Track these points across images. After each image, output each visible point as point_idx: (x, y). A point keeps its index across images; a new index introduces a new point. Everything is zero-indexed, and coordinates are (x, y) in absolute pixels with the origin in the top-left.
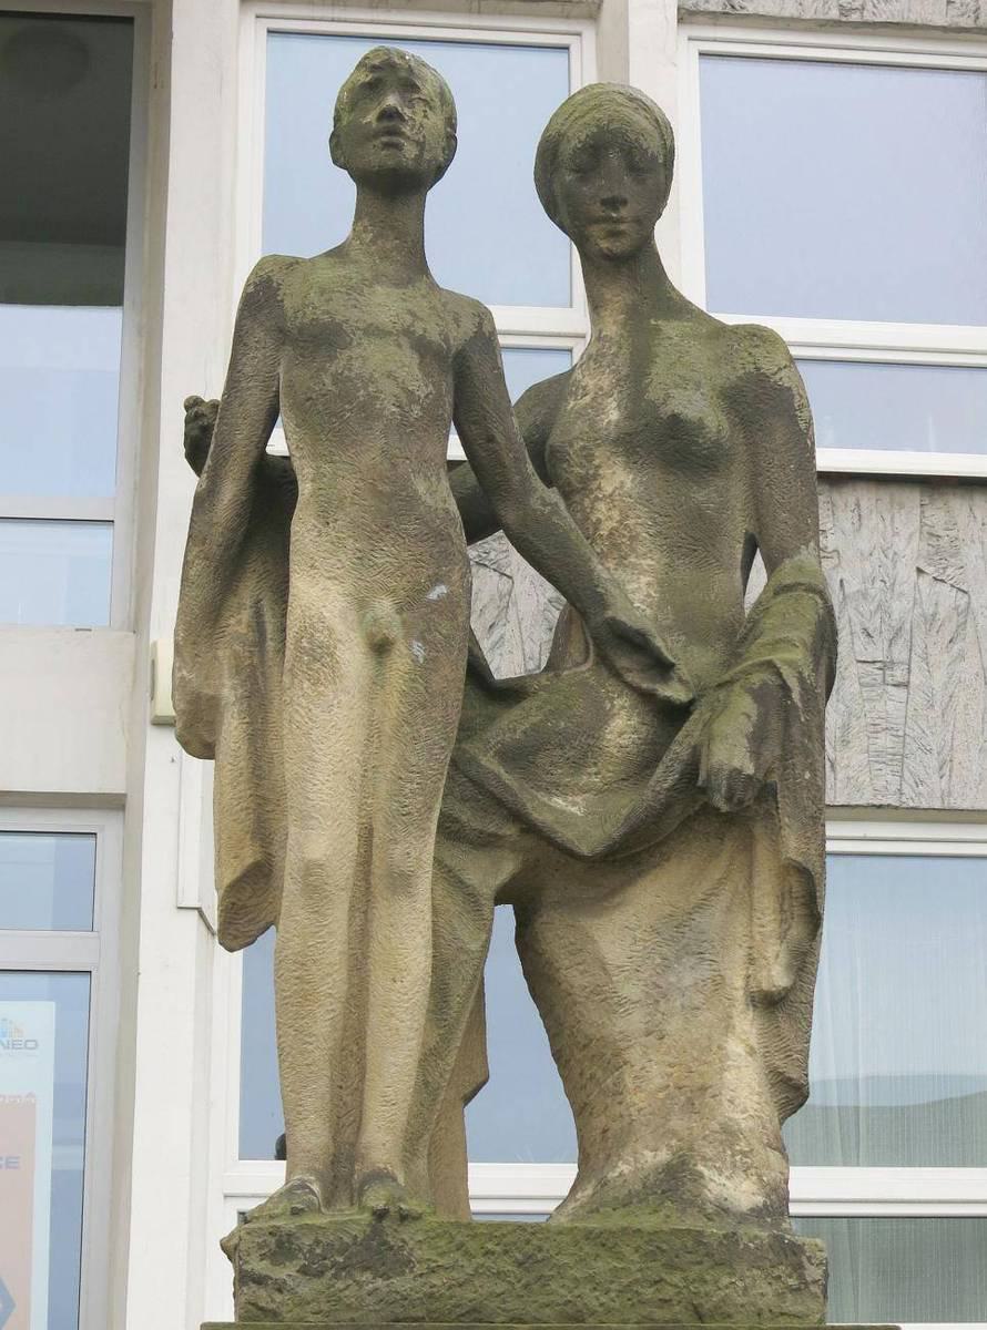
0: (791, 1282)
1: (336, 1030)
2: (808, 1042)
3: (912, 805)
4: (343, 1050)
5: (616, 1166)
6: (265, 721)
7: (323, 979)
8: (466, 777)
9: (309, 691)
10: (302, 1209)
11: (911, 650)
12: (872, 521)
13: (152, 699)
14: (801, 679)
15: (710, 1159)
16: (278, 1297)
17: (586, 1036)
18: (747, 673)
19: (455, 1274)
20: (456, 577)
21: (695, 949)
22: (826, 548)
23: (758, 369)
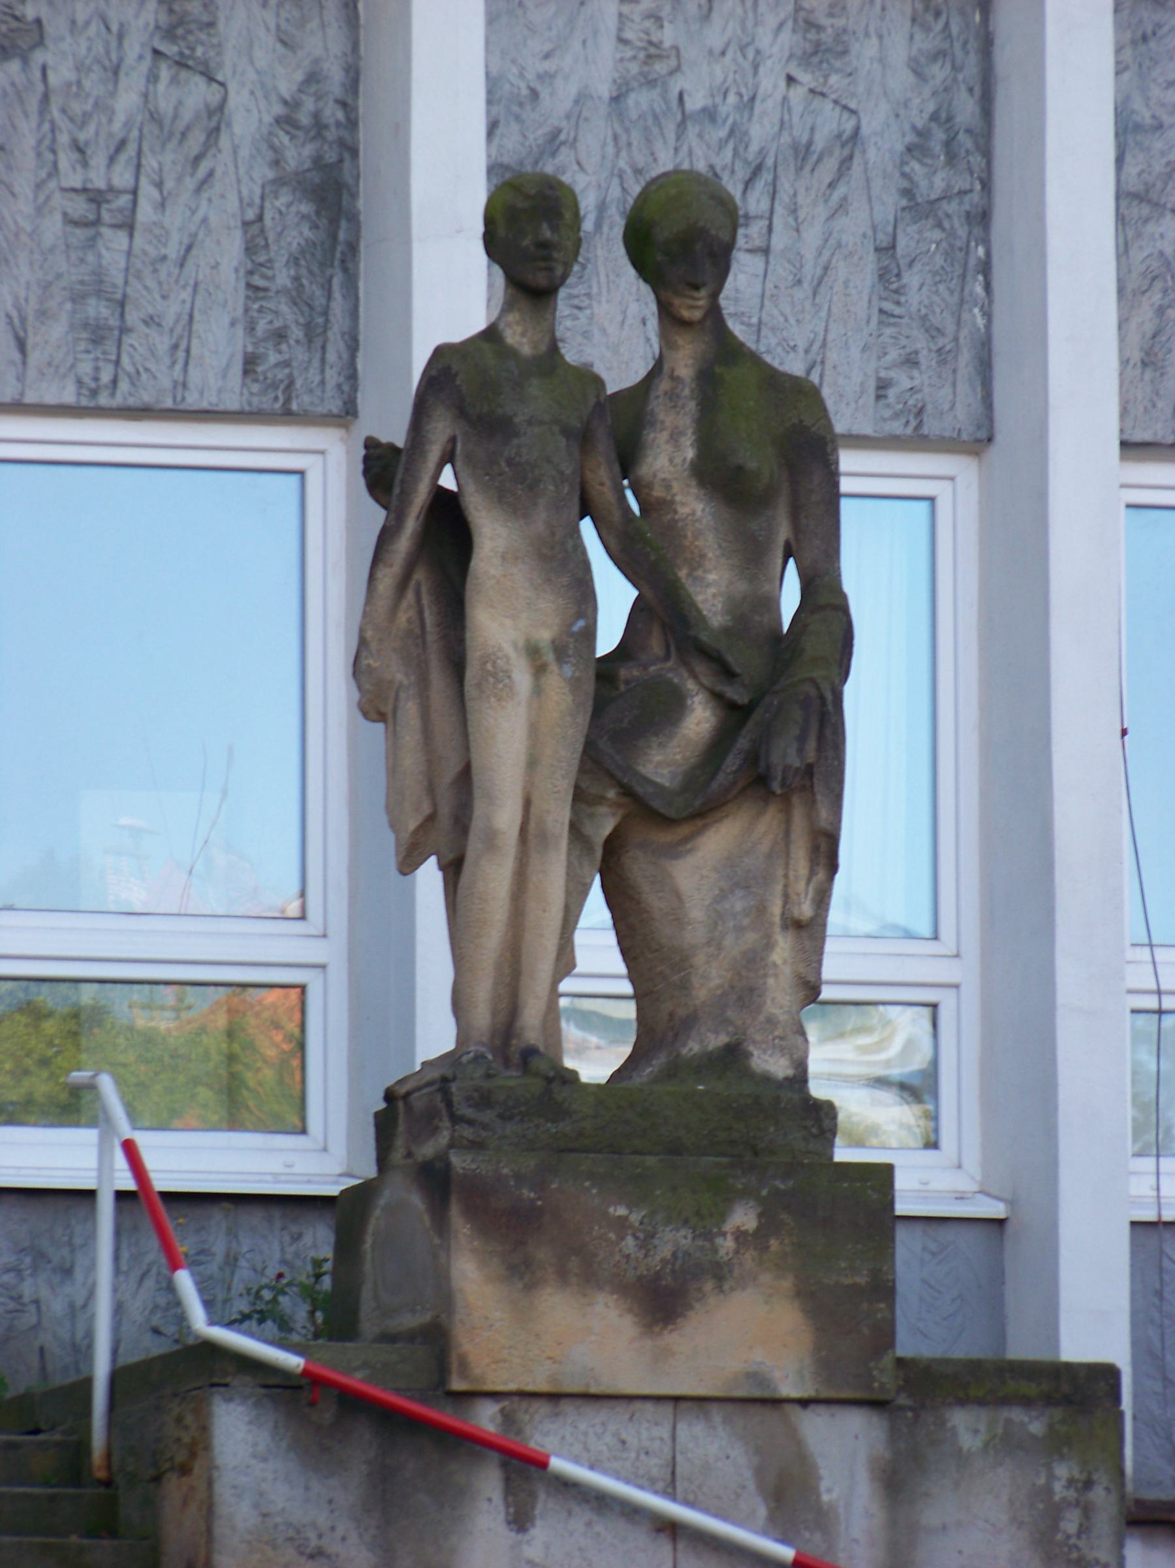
0: (814, 1131)
23: (801, 421)
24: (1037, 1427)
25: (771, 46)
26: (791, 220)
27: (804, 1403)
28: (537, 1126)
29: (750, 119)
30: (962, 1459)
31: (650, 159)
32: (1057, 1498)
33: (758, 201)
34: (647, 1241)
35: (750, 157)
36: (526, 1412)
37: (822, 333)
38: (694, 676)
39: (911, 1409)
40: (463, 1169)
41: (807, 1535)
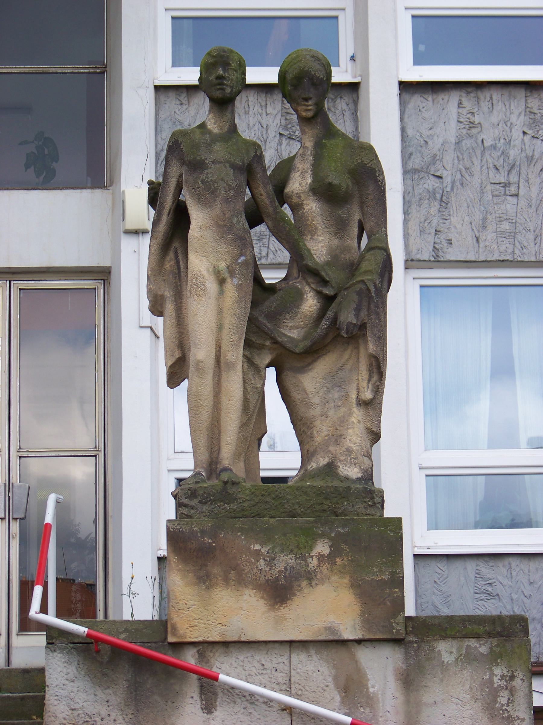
1: (210, 418)
2: (380, 417)
3: (519, 259)
4: (212, 425)
5: (311, 464)
6: (181, 303)
7: (204, 401)
8: (254, 324)
9: (196, 299)
10: (199, 482)
11: (519, 176)
12: (499, 107)
13: (123, 220)
14: (375, 286)
15: (342, 461)
16: (192, 511)
17: (301, 417)
18: (354, 284)
19: (252, 503)
20: (248, 253)
21: (339, 384)
22: (474, 122)
23: (362, 161)
24: (484, 650)
25: (517, 121)
26: (526, 184)
27: (359, 642)
28: (219, 507)
29: (509, 148)
30: (444, 667)
31: (471, 164)
32: (495, 685)
33: (514, 178)
34: (271, 561)
35: (510, 162)
36: (211, 651)
37: (540, 224)
38: (309, 284)
39: (416, 642)
40: (173, 528)
41: (362, 710)
